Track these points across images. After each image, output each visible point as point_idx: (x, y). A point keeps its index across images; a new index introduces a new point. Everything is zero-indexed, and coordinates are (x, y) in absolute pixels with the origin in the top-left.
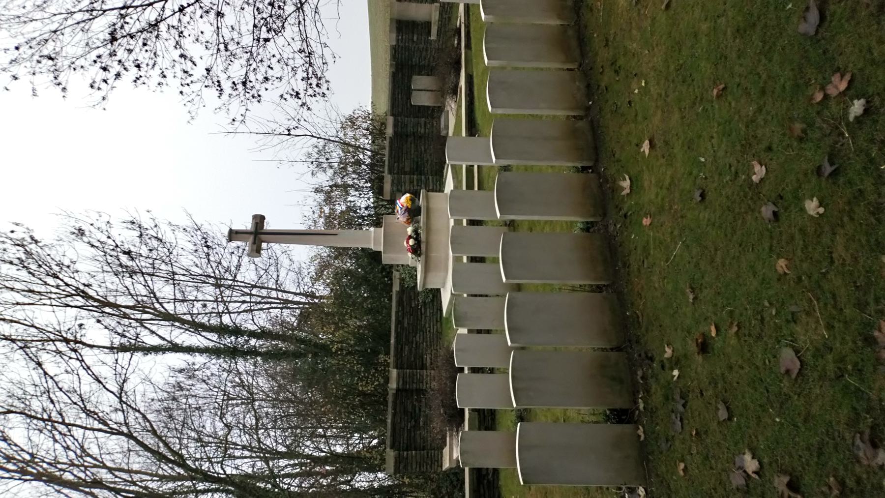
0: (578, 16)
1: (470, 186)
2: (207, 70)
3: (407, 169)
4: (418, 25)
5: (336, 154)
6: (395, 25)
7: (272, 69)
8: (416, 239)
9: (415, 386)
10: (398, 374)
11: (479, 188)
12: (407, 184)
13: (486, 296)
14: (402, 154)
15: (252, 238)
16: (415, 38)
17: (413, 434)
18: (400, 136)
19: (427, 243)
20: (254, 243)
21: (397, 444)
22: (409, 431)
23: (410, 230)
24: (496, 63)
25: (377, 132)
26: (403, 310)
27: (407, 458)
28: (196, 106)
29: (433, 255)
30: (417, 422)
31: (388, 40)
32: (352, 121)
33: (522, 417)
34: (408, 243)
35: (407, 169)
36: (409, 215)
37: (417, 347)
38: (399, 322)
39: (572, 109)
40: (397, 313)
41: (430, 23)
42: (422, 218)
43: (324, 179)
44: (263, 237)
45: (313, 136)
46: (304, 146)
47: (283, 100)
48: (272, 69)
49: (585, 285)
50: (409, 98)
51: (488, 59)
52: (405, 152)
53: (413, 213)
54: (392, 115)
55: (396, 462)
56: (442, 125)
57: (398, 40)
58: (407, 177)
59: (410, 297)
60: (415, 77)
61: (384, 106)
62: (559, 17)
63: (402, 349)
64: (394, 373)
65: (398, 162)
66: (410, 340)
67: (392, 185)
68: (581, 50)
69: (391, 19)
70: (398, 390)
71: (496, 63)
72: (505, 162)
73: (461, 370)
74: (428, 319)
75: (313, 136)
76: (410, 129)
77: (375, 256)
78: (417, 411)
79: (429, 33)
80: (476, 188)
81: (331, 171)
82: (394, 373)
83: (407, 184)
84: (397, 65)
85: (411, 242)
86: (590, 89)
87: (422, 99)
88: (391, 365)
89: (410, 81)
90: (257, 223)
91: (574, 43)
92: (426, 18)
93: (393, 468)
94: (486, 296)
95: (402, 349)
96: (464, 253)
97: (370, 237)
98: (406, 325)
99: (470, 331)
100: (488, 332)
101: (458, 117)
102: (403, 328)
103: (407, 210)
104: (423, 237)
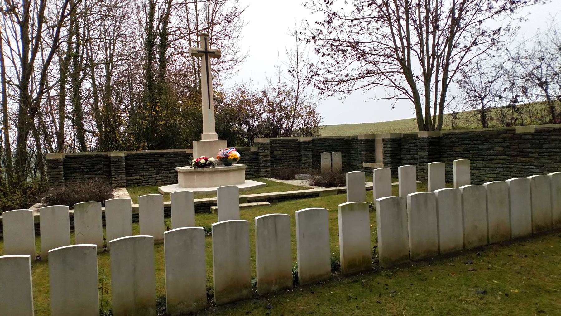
0: (262, 296)
1: (242, 200)
2: (335, 13)
3: (275, 153)
4: (372, 154)
5: (288, 103)
6: (371, 138)
7: (323, 56)
8: (205, 164)
9: (112, 169)
10: (121, 157)
11: (241, 207)
12: (263, 154)
13: (104, 226)
14: (279, 147)
15: (203, 50)
16: (363, 152)
17: (78, 171)
18: (298, 145)
19: (203, 172)
20: (199, 52)
21: (70, 160)
22: (80, 168)
23: (212, 159)
24: (409, 201)
25: (307, 131)
26: (172, 157)
27: (57, 168)
28: (312, 8)
29: (195, 177)
30: (87, 173)
31: (361, 134)
32: (312, 113)
33: (208, 232)
34: (203, 158)
35: (275, 153)
36: (223, 158)
37: (144, 169)
38: (162, 155)
39: (301, 272)
40: (169, 153)
41: (374, 162)
42: (223, 167)
43: (273, 96)
44: (204, 57)
45: (298, 87)
46: (291, 83)
47: (309, 66)
48: (323, 56)
49: (255, 272)
50: (327, 151)
51: (412, 196)
52: (288, 150)
53: (226, 161)
54: (313, 140)
55: (54, 160)
56: (301, 175)
57: (361, 141)
58: (269, 153)
59: (182, 162)
60: (340, 154)
61: (324, 134)
62: (261, 280)
63: (142, 158)
64: (122, 154)
65: (280, 146)
66: (149, 164)
67: (262, 143)
68: (229, 303)
69: (375, 135)
70: (110, 158)
71: (409, 201)
72: (378, 208)
73: (103, 205)
74: (166, 175)
75: (298, 87)
76: (303, 153)
77: (198, 136)
78: (95, 173)
79: (367, 162)
80: (393, 184)
81: (278, 101)
82: (122, 154)
83: (263, 154)
84: (350, 141)
85: (203, 161)
86: (267, 295)
87: (325, 159)
88: (129, 152)
89: (338, 150)
90: (214, 53)
91: (236, 296)
92: (377, 160)
93: (50, 159)
94: (104, 226)
95: (142, 158)
96: (219, 198)
97: (209, 132)
98: (160, 160)
99: (37, 218)
100: (72, 228)
101: (299, 188)
102: (158, 158)
103: (226, 157)
104: (206, 169)
